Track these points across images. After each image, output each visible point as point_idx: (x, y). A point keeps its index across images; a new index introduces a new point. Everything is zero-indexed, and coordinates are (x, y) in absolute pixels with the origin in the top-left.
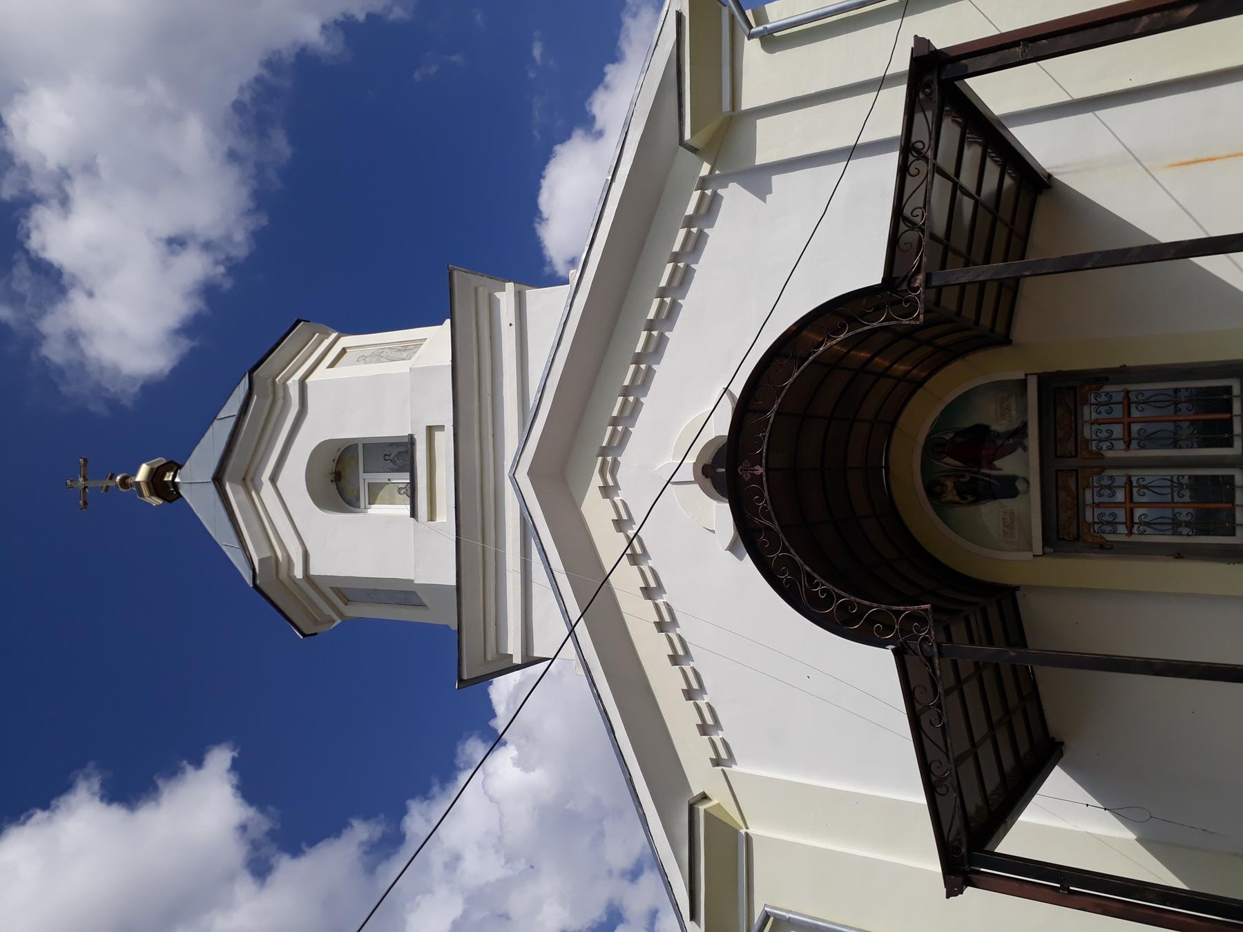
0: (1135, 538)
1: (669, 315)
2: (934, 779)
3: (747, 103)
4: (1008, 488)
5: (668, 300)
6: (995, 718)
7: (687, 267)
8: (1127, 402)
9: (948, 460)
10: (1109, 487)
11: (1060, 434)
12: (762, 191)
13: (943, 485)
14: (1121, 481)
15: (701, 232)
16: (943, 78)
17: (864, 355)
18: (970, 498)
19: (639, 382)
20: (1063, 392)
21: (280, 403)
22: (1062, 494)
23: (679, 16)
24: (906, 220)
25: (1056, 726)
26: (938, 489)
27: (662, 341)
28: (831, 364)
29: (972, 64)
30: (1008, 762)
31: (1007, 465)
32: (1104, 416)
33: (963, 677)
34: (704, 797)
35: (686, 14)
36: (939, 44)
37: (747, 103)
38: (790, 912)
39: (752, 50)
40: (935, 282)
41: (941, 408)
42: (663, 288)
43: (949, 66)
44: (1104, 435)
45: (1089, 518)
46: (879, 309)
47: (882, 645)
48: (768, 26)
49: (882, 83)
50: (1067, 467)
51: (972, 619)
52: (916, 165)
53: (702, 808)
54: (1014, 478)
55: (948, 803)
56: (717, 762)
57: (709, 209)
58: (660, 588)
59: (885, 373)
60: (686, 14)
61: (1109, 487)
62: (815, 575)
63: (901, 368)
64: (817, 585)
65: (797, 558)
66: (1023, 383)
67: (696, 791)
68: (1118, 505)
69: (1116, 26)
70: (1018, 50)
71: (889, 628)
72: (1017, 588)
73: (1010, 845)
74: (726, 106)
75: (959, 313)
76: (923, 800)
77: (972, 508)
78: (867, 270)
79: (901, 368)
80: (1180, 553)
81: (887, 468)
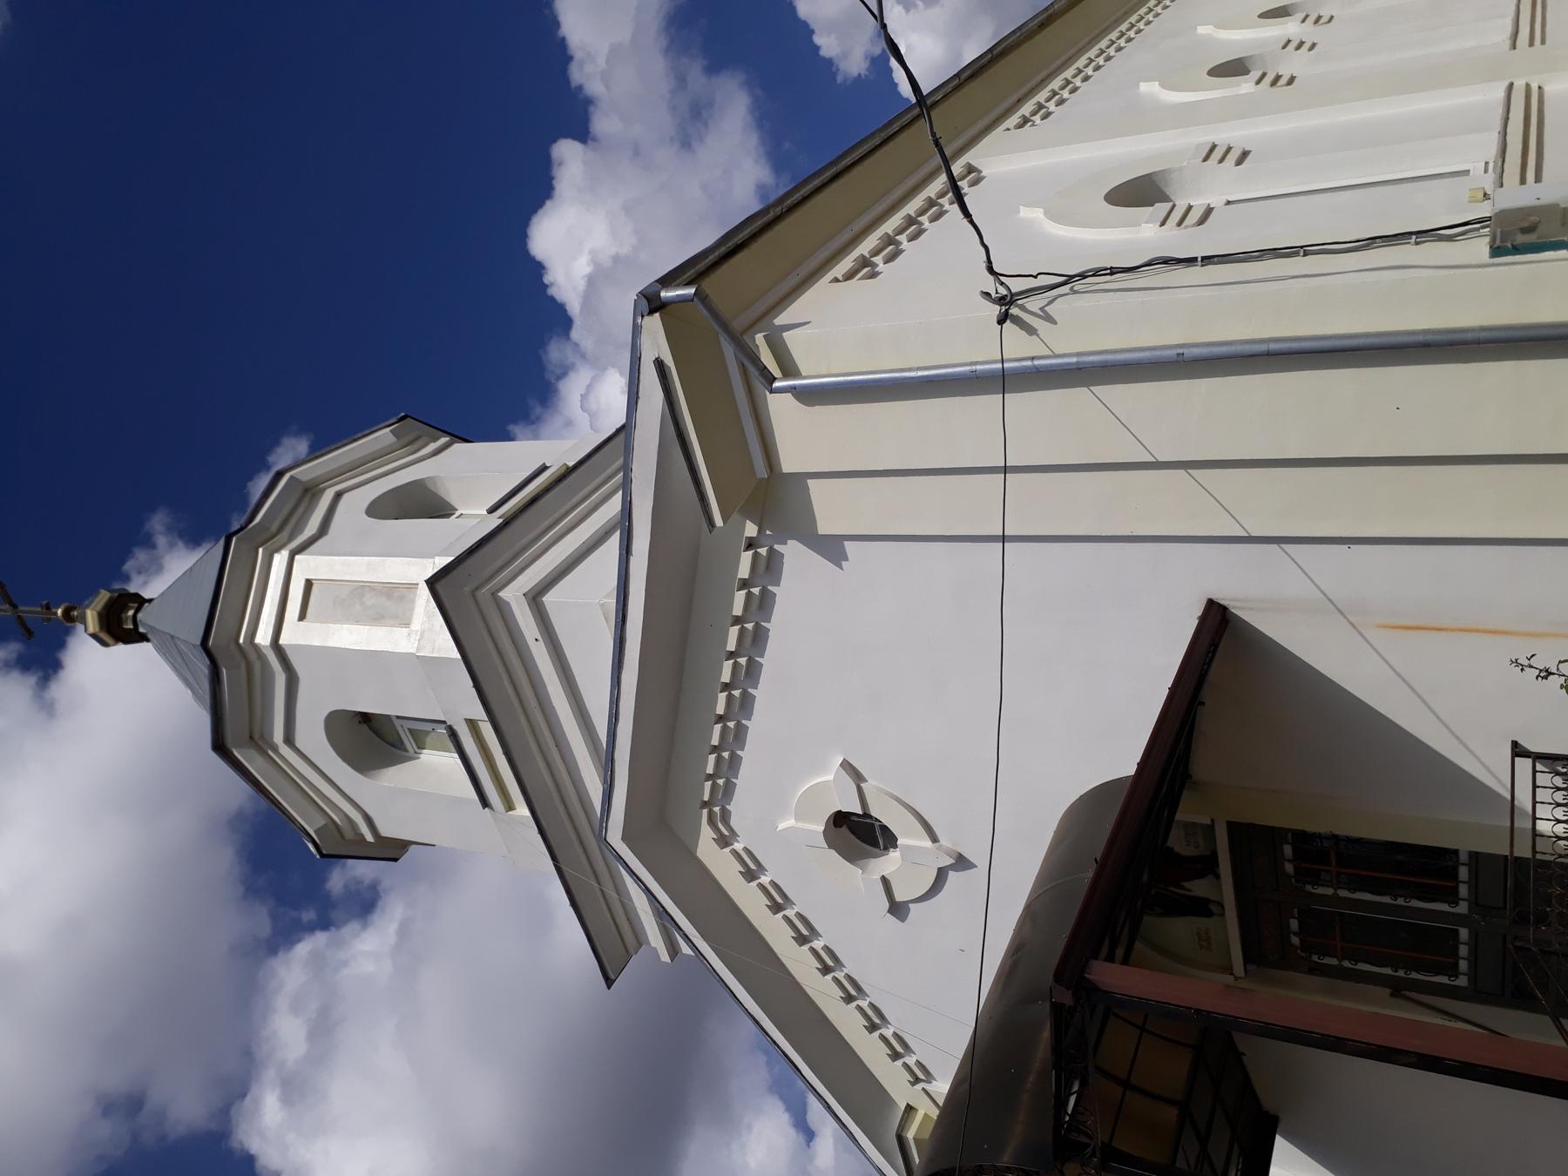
21: (257, 666)
23: (659, 364)
25: (1268, 1102)
35: (669, 361)
54: (1206, 901)
57: (769, 568)
58: (814, 932)
60: (669, 361)
74: (761, 471)
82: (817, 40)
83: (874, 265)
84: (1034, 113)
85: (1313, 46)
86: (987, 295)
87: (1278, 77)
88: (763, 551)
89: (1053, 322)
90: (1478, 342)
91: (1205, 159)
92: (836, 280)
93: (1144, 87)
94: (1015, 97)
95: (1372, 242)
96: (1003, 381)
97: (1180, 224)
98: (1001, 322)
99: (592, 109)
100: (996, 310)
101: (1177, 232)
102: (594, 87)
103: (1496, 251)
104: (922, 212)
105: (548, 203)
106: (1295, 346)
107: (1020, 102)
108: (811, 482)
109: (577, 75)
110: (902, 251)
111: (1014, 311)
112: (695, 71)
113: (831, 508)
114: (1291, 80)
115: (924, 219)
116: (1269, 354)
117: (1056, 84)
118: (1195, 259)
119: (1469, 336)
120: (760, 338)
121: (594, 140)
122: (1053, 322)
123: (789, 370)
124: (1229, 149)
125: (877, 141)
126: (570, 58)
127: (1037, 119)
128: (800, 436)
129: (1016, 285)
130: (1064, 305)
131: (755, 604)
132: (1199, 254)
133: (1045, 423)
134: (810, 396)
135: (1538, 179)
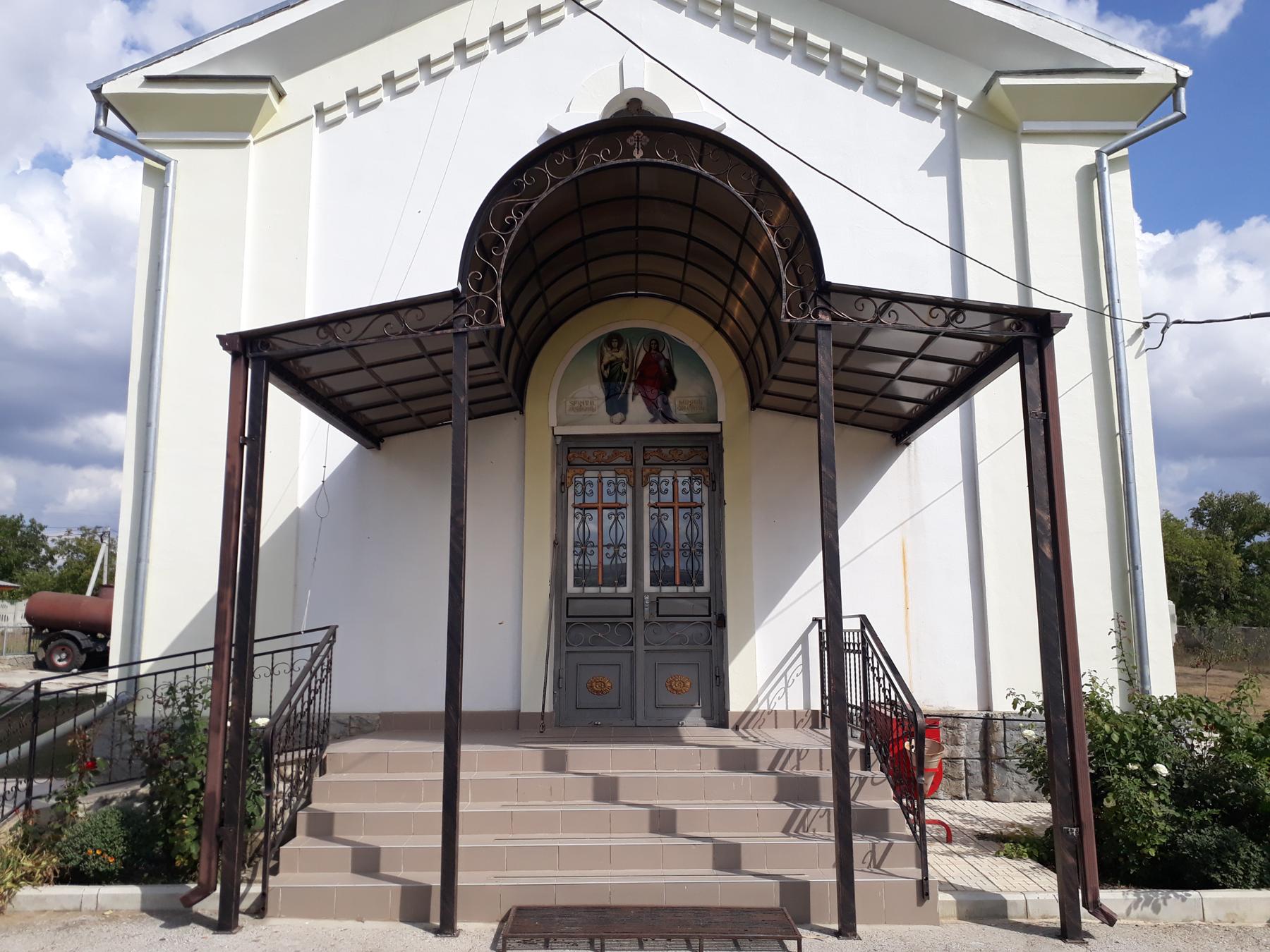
0: (571, 511)
1: (810, 60)
2: (332, 326)
3: (1027, 148)
4: (616, 404)
5: (827, 58)
6: (398, 388)
7: (861, 81)
8: (692, 506)
9: (643, 354)
10: (616, 490)
11: (665, 451)
12: (931, 166)
13: (619, 348)
14: (622, 500)
15: (896, 97)
16: (1025, 341)
17: (753, 271)
18: (606, 373)
19: (737, 23)
20: (704, 455)
22: (609, 452)
23: (1137, 72)
24: (887, 306)
25: (391, 443)
26: (615, 344)
27: (782, 51)
28: (745, 235)
29: (1033, 370)
30: (356, 400)
31: (637, 407)
32: (681, 487)
33: (434, 358)
34: (281, 95)
35: (1139, 80)
36: (1059, 339)
37: (1027, 148)
38: (174, 187)
39: (1085, 154)
40: (822, 333)
41: (694, 346)
42: (840, 53)
43: (1035, 347)
44: (663, 486)
45: (588, 474)
46: (799, 280)
47: (462, 279)
48: (1106, 173)
49: (1025, 285)
50: (637, 457)
51: (491, 370)
52: (941, 315)
53: (268, 91)
55: (311, 339)
56: (320, 110)
57: (921, 106)
59: (731, 291)
60: (1139, 80)
61: (616, 490)
62: (528, 213)
63: (737, 309)
64: (519, 215)
65: (545, 195)
66: (714, 420)
67: (286, 85)
68: (600, 496)
69: (1046, 494)
70: (1039, 410)
71: (479, 286)
72: (522, 412)
73: (278, 398)
74: (1028, 126)
75: (766, 392)
76: (310, 313)
77: (597, 376)
78: (842, 265)
79: (737, 309)
80: (559, 546)
81: (636, 295)
99: (647, 105)
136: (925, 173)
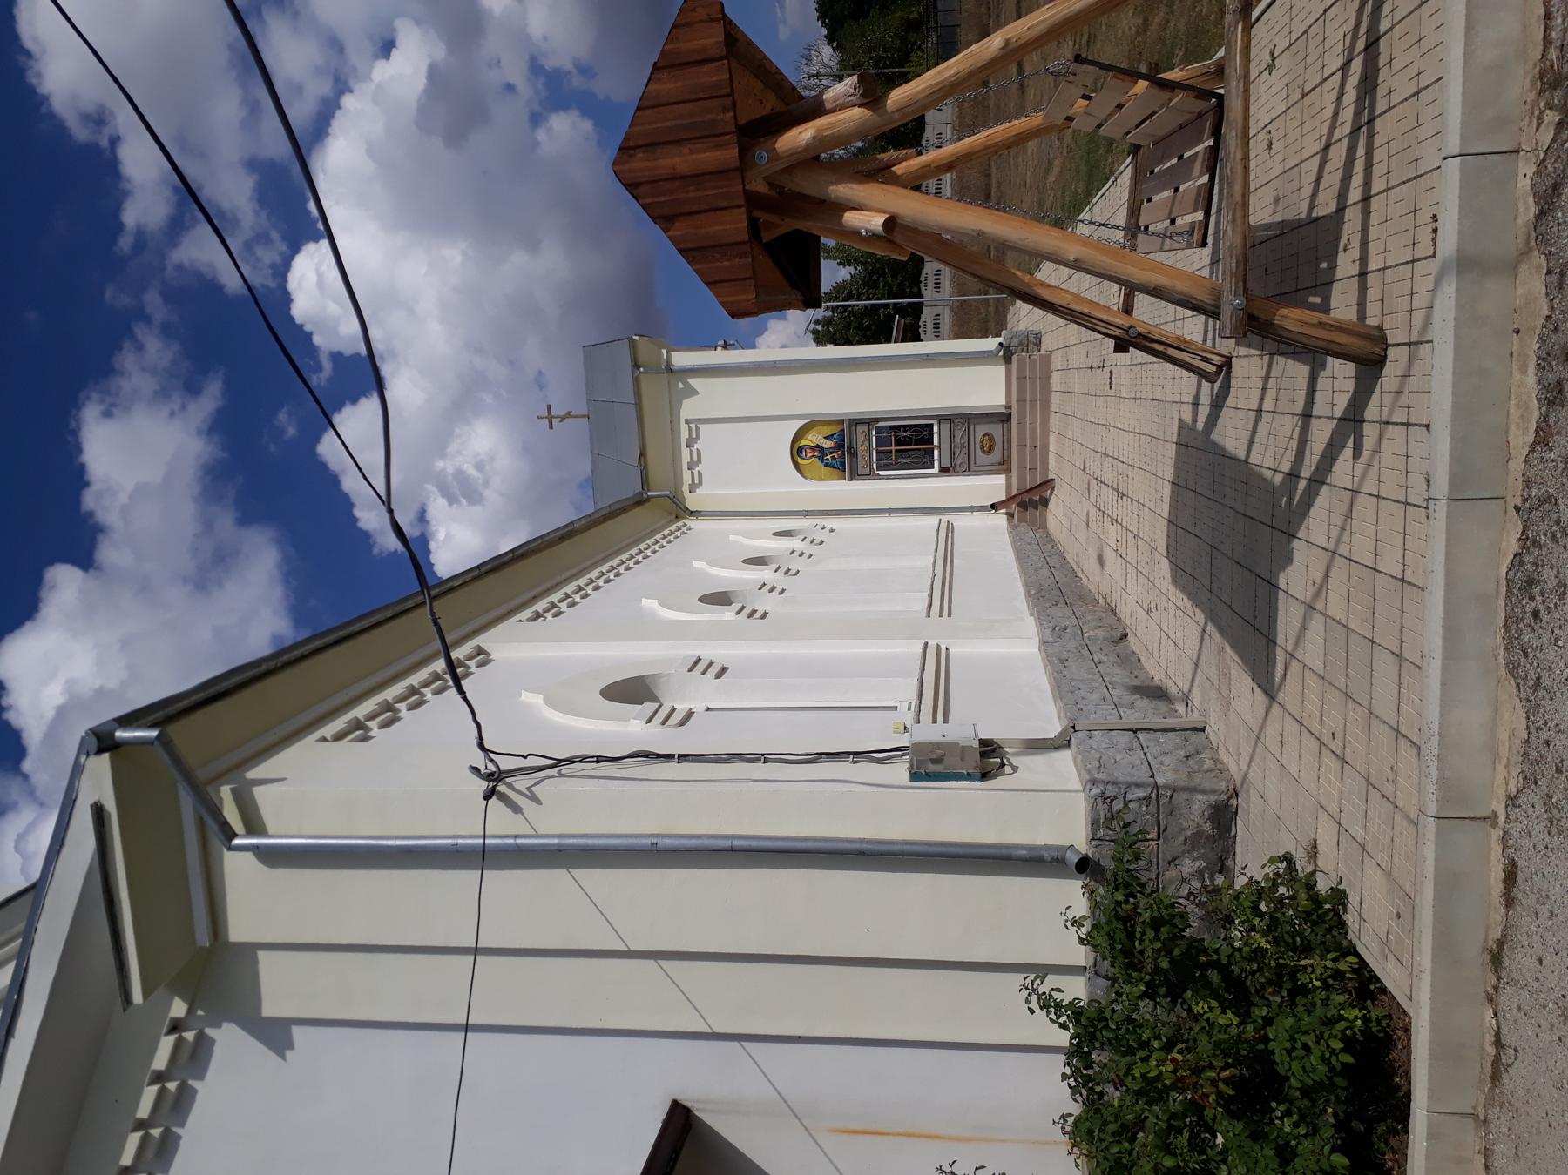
23: (98, 812)
35: (111, 806)
57: (193, 1058)
60: (111, 806)
74: (203, 938)
82: (358, 513)
83: (368, 729)
84: (547, 611)
85: (783, 591)
86: (476, 770)
87: (754, 611)
88: (190, 1036)
89: (539, 802)
90: (903, 854)
91: (690, 670)
92: (324, 739)
93: (645, 602)
94: (529, 595)
95: (819, 757)
96: (483, 857)
97: (664, 723)
98: (487, 797)
99: (100, 537)
100: (483, 785)
101: (660, 729)
102: (108, 515)
103: (914, 776)
104: (426, 684)
105: (28, 625)
106: (754, 844)
107: (535, 599)
108: (261, 955)
109: (89, 500)
110: (399, 719)
111: (501, 788)
112: (226, 520)
113: (281, 988)
114: (764, 616)
115: (427, 691)
116: (731, 850)
117: (569, 589)
118: (672, 756)
119: (896, 848)
120: (226, 791)
121: (98, 568)
122: (539, 802)
123: (254, 825)
124: (711, 664)
125: (390, 613)
126: (87, 484)
127: (549, 615)
128: (254, 901)
129: (506, 764)
130: (551, 788)
131: (167, 1104)
132: (677, 752)
133: (522, 904)
134: (273, 857)
135: (946, 721)
136: (289, 1054)
